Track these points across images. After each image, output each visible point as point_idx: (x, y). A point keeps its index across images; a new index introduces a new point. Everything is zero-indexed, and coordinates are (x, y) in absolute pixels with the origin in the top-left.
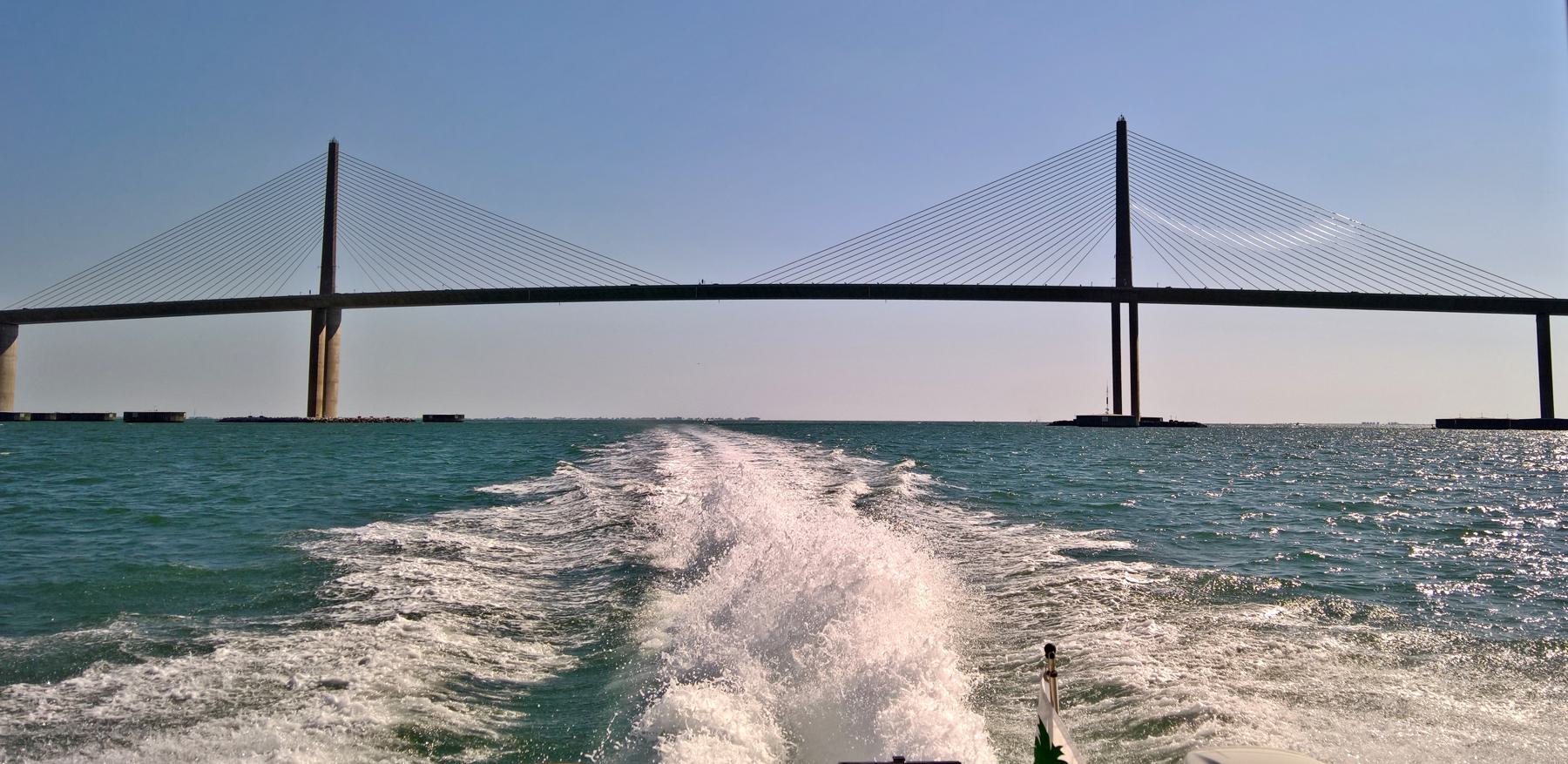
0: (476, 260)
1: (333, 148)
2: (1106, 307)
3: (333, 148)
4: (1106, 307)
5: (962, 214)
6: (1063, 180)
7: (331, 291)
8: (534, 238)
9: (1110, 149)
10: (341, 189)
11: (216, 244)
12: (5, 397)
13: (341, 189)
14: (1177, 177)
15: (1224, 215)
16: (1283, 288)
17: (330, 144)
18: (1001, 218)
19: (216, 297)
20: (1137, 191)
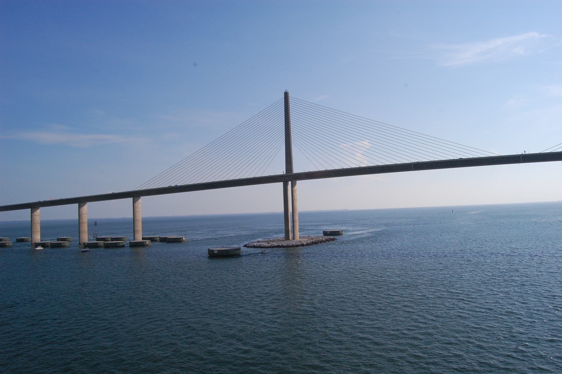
0: (363, 133)
1: (286, 94)
2: (280, 185)
3: (286, 94)
4: (280, 185)
5: (217, 154)
6: (244, 139)
7: (292, 172)
8: (310, 128)
9: (282, 116)
10: (292, 105)
11: (187, 167)
12: (138, 232)
13: (292, 105)
14: (187, 162)
15: (306, 129)
16: (398, 163)
17: (284, 93)
18: (266, 139)
19: (192, 183)
20: (295, 124)
